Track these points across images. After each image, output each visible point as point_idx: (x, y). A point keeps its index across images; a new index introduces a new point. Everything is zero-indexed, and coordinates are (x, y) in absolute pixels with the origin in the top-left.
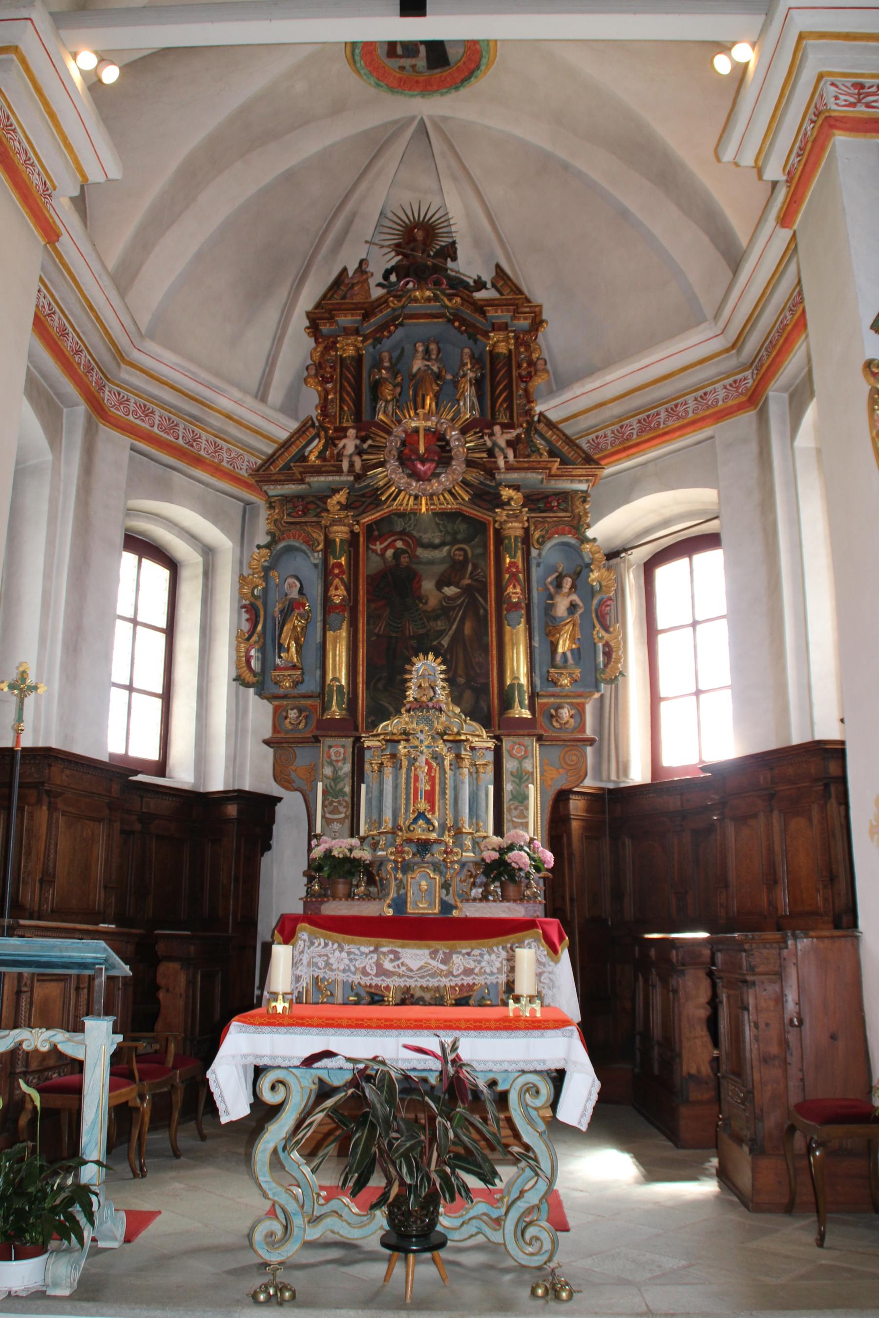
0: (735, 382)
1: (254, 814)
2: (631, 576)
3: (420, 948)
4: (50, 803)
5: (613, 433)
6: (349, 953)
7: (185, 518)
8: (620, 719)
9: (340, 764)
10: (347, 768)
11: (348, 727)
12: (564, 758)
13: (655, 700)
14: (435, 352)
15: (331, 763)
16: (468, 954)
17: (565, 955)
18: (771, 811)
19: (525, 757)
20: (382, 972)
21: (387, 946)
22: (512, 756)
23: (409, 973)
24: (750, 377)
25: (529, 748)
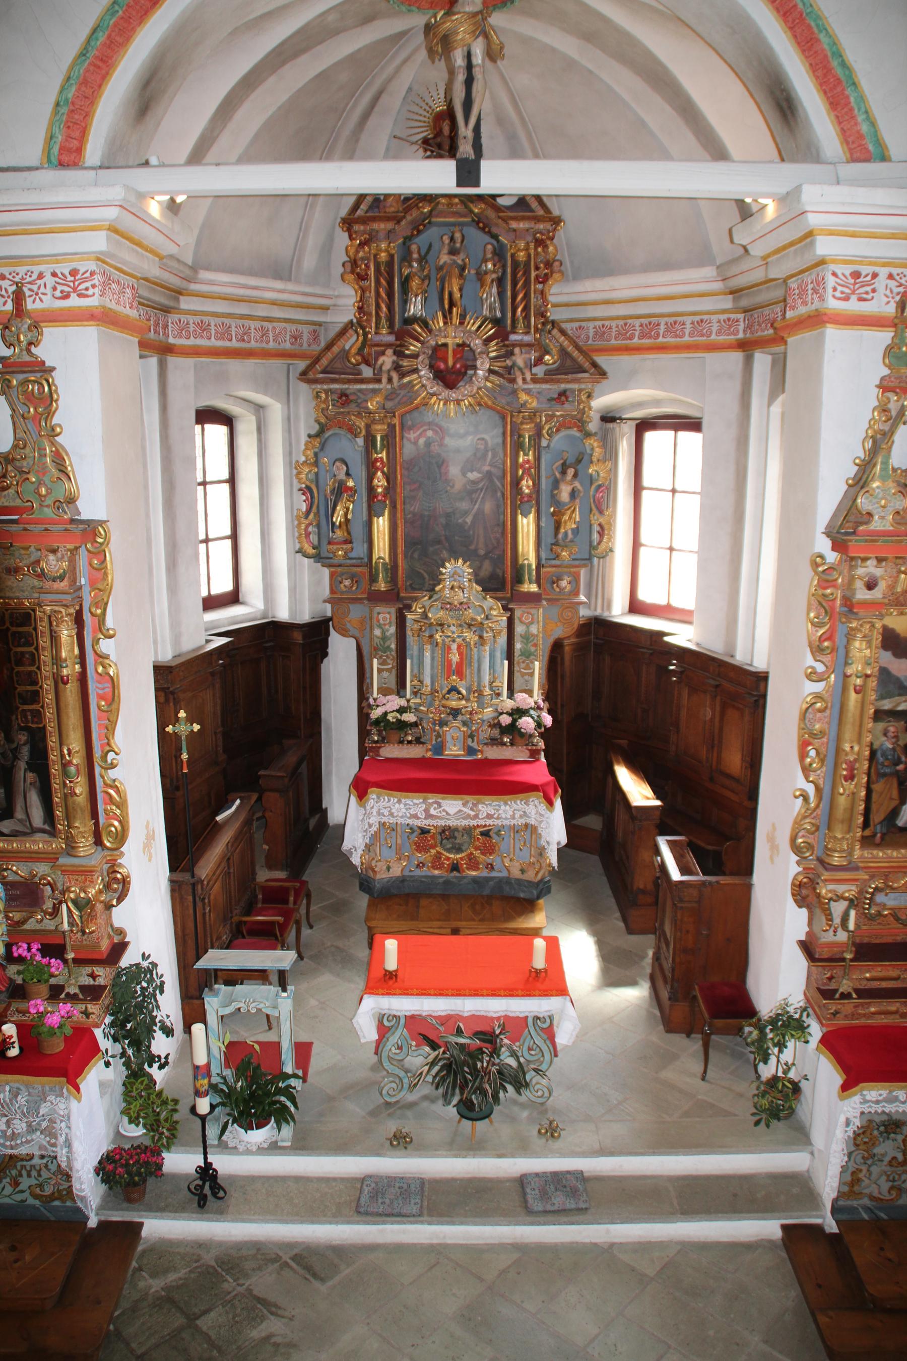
0: (729, 319)
1: (314, 637)
2: (625, 442)
3: (455, 800)
4: (174, 699)
5: (617, 327)
6: (405, 805)
7: (239, 388)
8: (606, 585)
9: (387, 627)
10: (392, 630)
11: (392, 596)
12: (561, 614)
13: (636, 545)
14: (459, 240)
15: (380, 626)
16: (490, 805)
17: (558, 803)
18: (716, 696)
19: (532, 623)
20: (428, 816)
21: (432, 798)
22: (521, 622)
23: (448, 817)
24: (742, 320)
25: (536, 616)
